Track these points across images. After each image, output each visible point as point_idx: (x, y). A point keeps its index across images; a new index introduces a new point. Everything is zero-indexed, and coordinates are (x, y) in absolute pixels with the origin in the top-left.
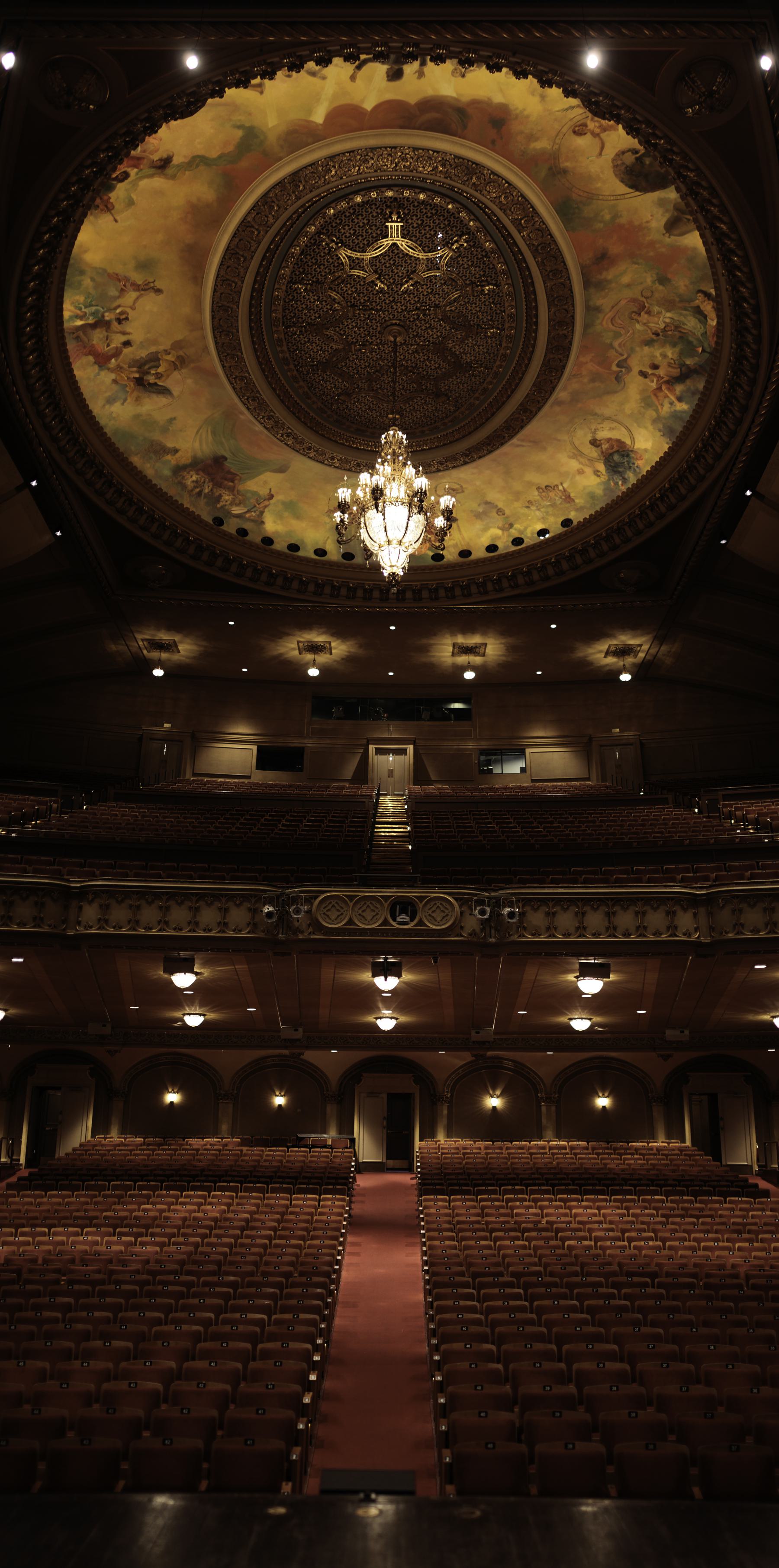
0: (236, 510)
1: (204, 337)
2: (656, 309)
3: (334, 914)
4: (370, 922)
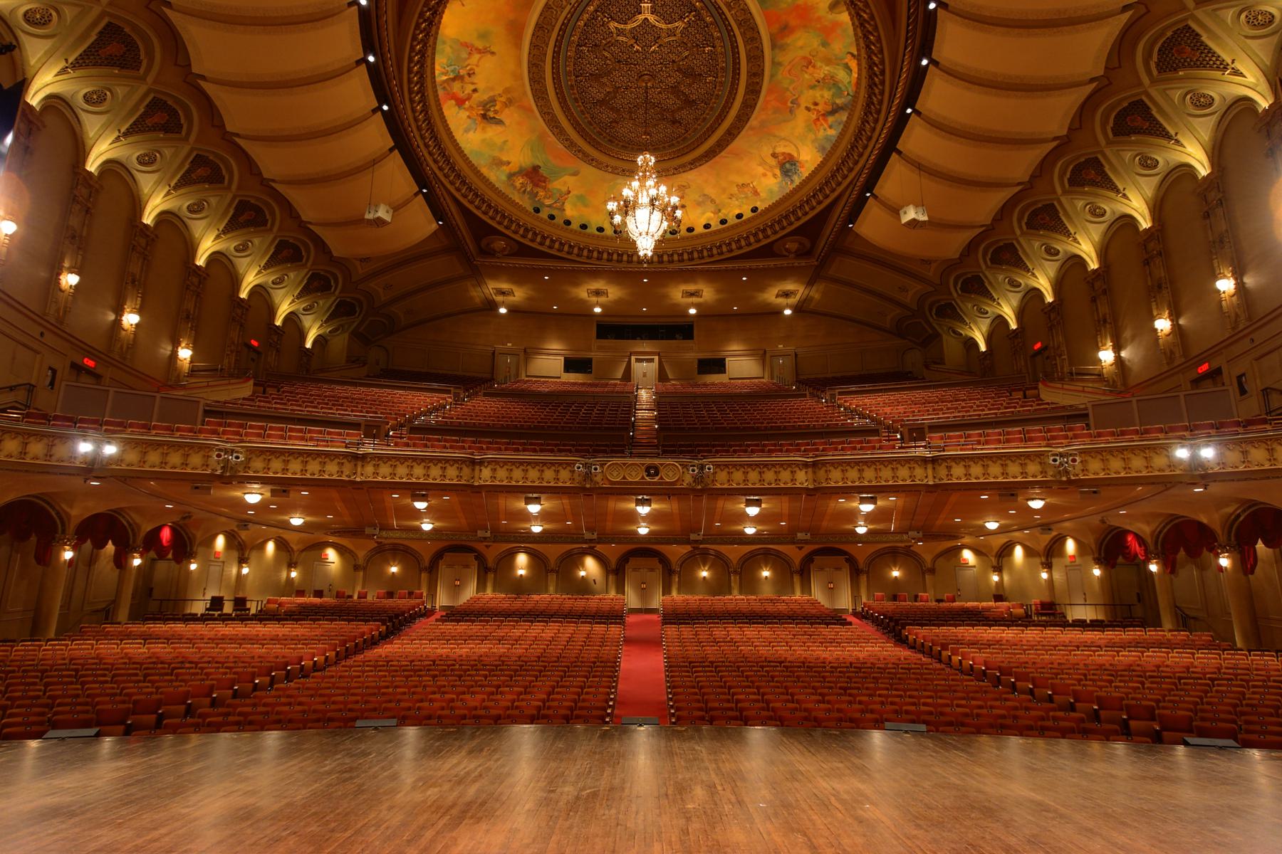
0: (548, 202)
1: (523, 85)
2: (819, 64)
3: (615, 474)
4: (636, 476)
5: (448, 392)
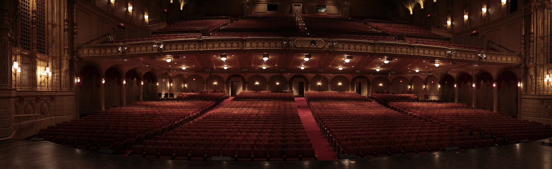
5: (228, 19)
